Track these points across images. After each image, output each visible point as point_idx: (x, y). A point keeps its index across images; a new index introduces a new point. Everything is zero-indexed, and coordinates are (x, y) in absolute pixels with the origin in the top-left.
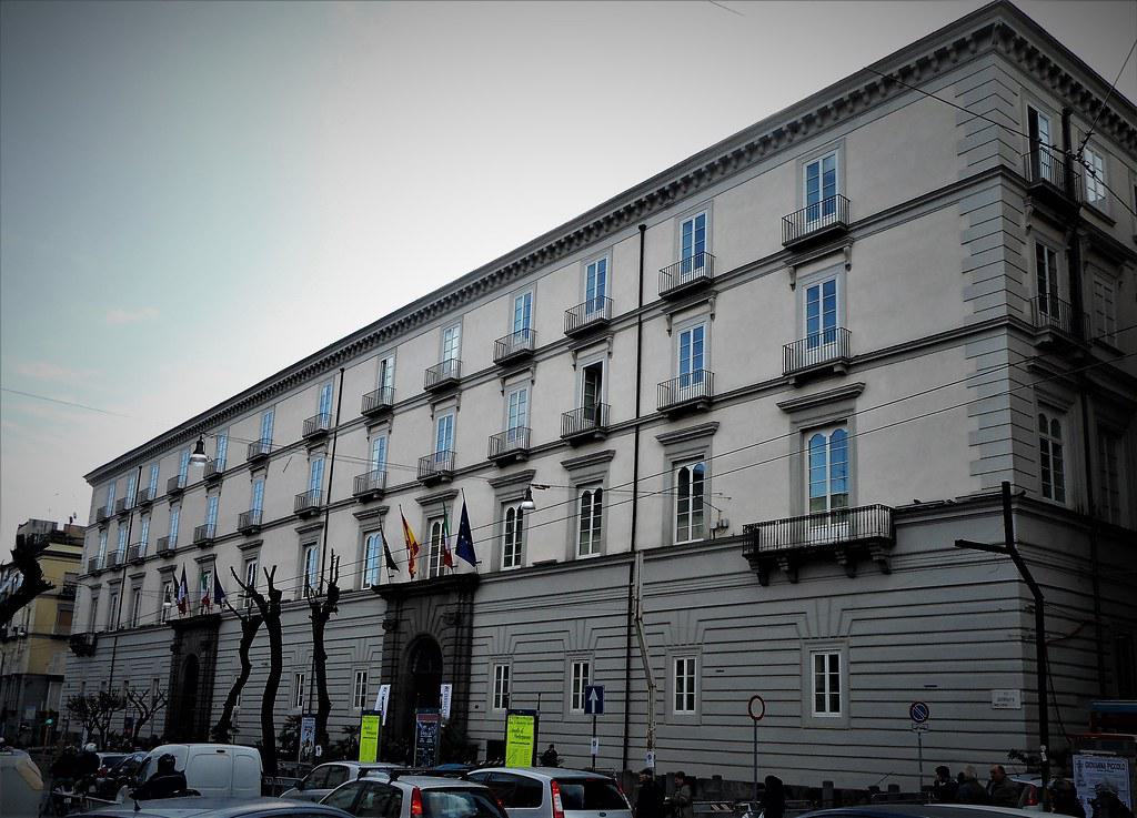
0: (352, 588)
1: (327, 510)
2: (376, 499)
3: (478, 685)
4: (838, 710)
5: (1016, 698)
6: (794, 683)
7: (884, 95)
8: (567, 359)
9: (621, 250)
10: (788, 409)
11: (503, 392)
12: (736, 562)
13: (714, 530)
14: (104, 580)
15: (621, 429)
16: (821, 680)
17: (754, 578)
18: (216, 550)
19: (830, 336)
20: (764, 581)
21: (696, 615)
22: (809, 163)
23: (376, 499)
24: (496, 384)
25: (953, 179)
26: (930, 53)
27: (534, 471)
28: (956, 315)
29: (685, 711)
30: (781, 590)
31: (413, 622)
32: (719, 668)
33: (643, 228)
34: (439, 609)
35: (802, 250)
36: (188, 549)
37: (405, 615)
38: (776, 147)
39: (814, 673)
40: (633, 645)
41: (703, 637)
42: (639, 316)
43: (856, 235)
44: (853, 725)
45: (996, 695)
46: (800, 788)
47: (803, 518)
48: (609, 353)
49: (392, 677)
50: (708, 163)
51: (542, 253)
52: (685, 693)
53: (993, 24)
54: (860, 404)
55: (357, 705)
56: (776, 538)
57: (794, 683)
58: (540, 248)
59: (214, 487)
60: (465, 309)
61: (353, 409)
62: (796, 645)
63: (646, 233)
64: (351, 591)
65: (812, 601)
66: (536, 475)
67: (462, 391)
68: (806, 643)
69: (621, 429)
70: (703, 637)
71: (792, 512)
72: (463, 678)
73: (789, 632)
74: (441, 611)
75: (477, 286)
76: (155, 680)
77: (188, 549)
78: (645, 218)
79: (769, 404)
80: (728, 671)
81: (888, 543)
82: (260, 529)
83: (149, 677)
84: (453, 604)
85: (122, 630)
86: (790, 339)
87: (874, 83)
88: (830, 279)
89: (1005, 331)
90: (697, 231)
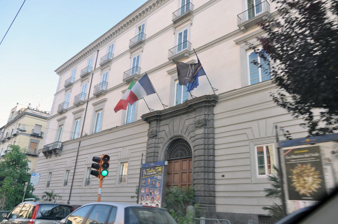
0: (68, 140)
6: (247, 162)
11: (174, 33)
21: (128, 148)
27: (66, 117)
34: (187, 121)
35: (177, 22)
37: (161, 129)
38: (146, 14)
40: (279, 134)
41: (130, 155)
44: (128, 186)
46: (226, 214)
48: (110, 69)
50: (139, 13)
54: (107, 103)
57: (247, 162)
59: (68, 90)
60: (77, 65)
61: (78, 76)
62: (247, 143)
63: (99, 52)
64: (68, 141)
65: (256, 122)
66: (67, 118)
68: (252, 142)
70: (130, 155)
73: (244, 137)
74: (191, 121)
76: (67, 170)
79: (231, 42)
81: (61, 149)
83: (117, 162)
84: (199, 115)
85: (86, 135)
88: (138, 55)
90: (141, 29)
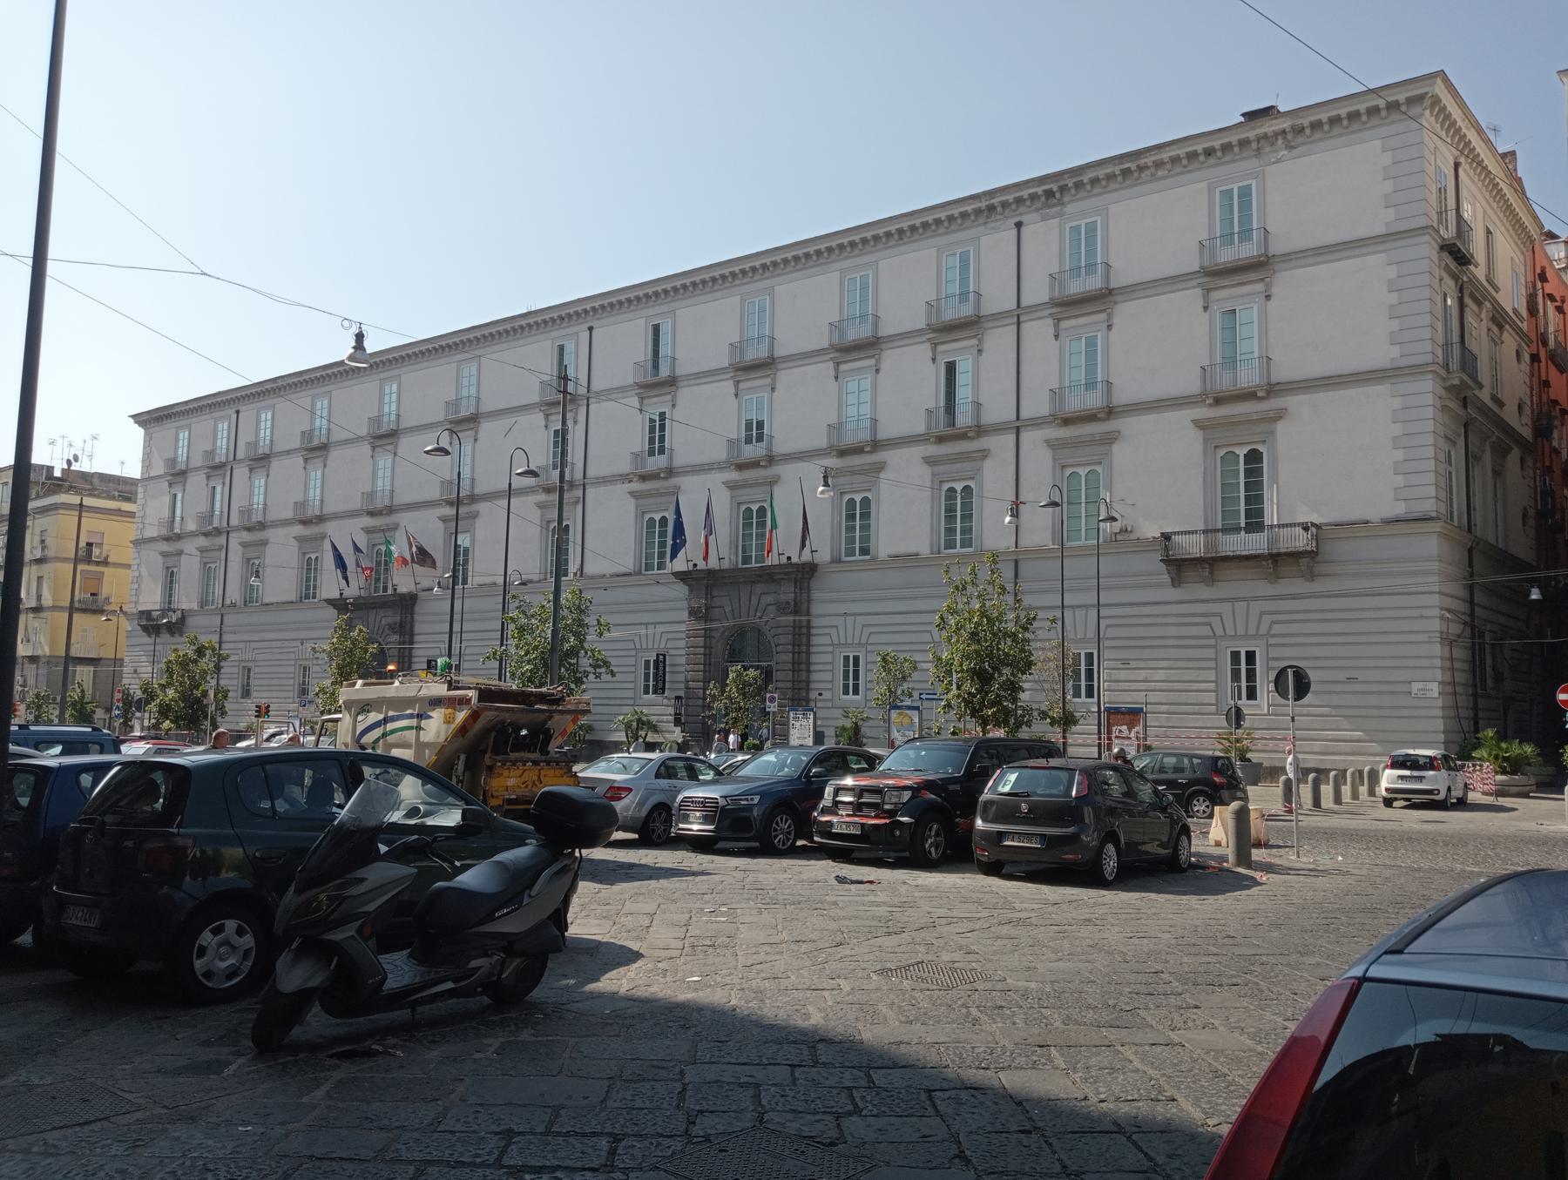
1: (228, 533)
2: (763, 466)
3: (818, 674)
4: (858, 694)
5: (1434, 689)
7: (947, 228)
8: (925, 350)
9: (995, 243)
10: (929, 461)
12: (1154, 561)
13: (1116, 534)
14: (190, 546)
15: (999, 428)
16: (846, 673)
17: (1166, 578)
18: (270, 534)
19: (662, 451)
20: (1176, 582)
22: (1224, 188)
23: (763, 466)
24: (728, 386)
25: (1379, 229)
26: (1343, 112)
28: (1382, 354)
29: (851, 697)
30: (1196, 590)
31: (728, 609)
32: (1126, 662)
33: (1019, 225)
34: (763, 597)
36: (285, 523)
38: (1089, 192)
39: (842, 668)
42: (1018, 316)
43: (1118, 298)
45: (1415, 687)
47: (1215, 531)
49: (705, 665)
51: (888, 235)
52: (851, 682)
53: (1426, 93)
55: (846, 692)
56: (1194, 546)
58: (764, 261)
60: (404, 369)
67: (778, 370)
69: (999, 428)
71: (1206, 522)
72: (803, 667)
75: (797, 259)
77: (285, 523)
78: (1021, 214)
80: (1133, 664)
82: (473, 499)
84: (787, 593)
86: (637, 449)
87: (1397, 101)
89: (1430, 376)
